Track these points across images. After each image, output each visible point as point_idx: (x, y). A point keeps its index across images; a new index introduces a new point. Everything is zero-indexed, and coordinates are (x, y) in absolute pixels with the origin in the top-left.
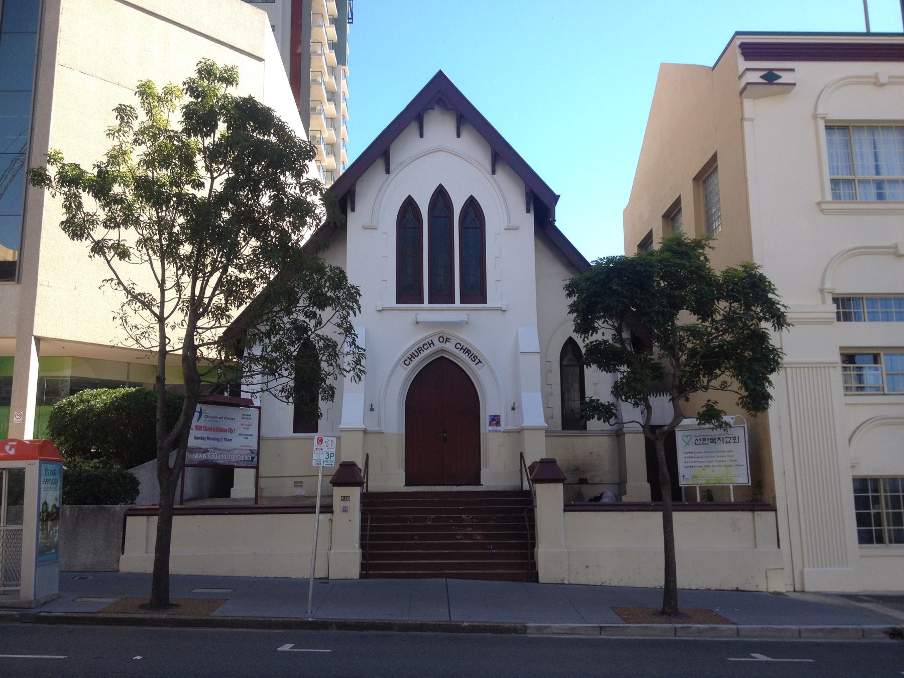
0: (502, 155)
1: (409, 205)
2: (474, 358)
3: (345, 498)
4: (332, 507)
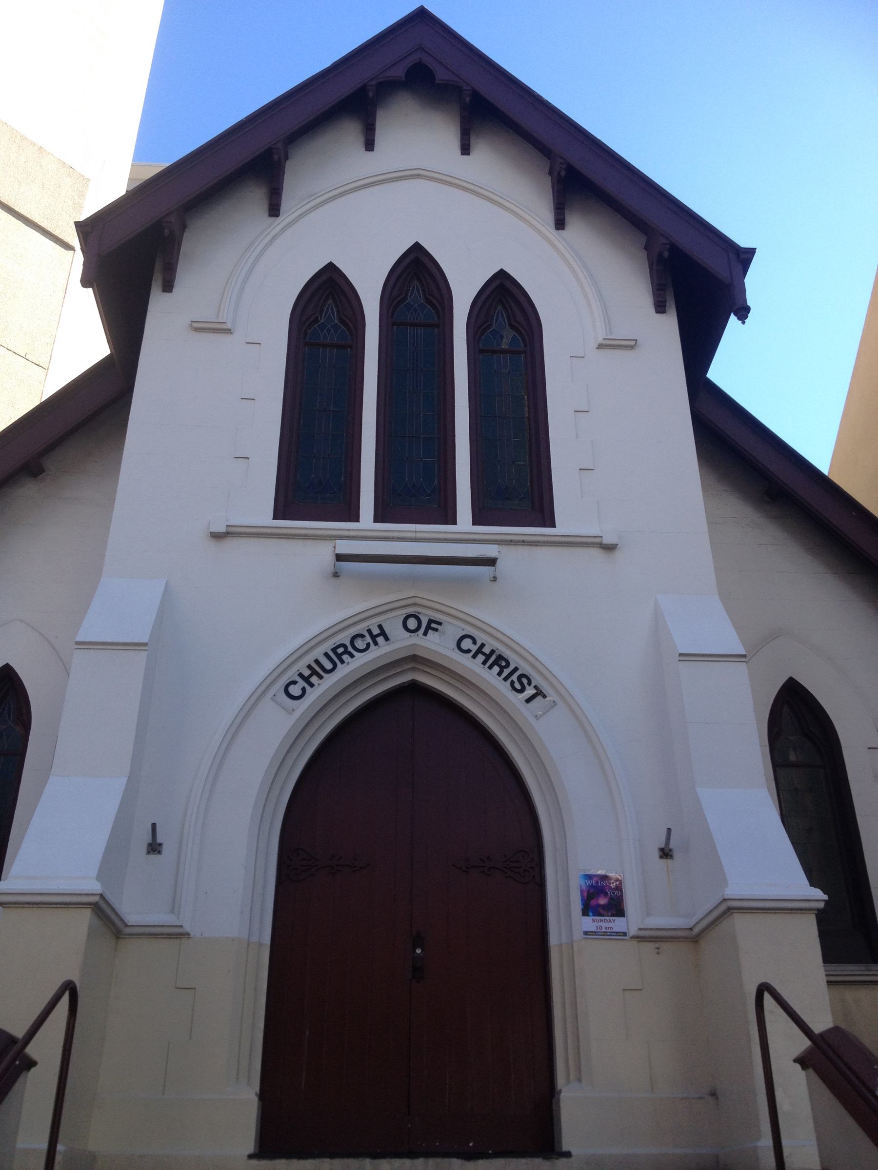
0: (586, 179)
1: (328, 292)
2: (520, 682)
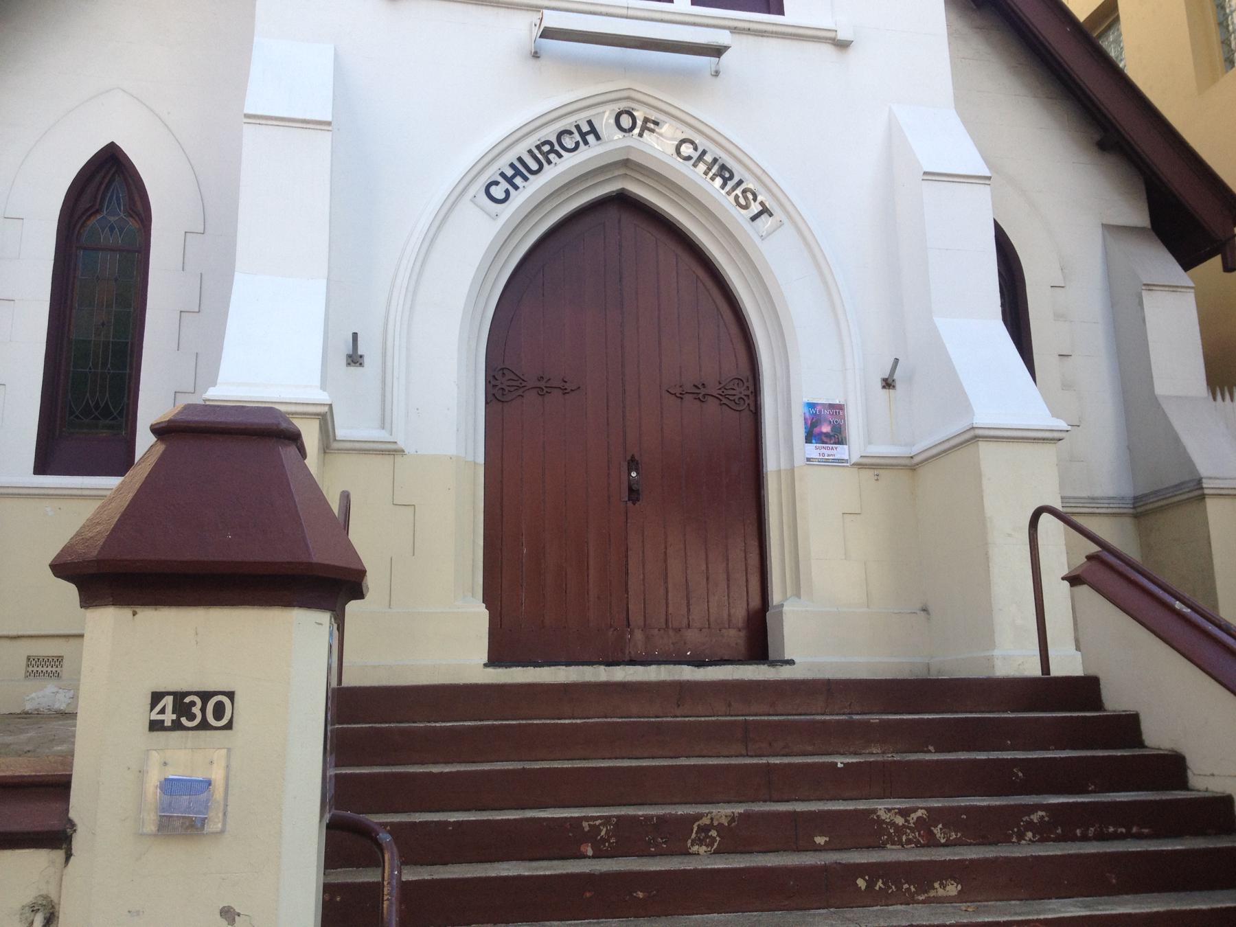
3: (190, 710)
4: (59, 787)
